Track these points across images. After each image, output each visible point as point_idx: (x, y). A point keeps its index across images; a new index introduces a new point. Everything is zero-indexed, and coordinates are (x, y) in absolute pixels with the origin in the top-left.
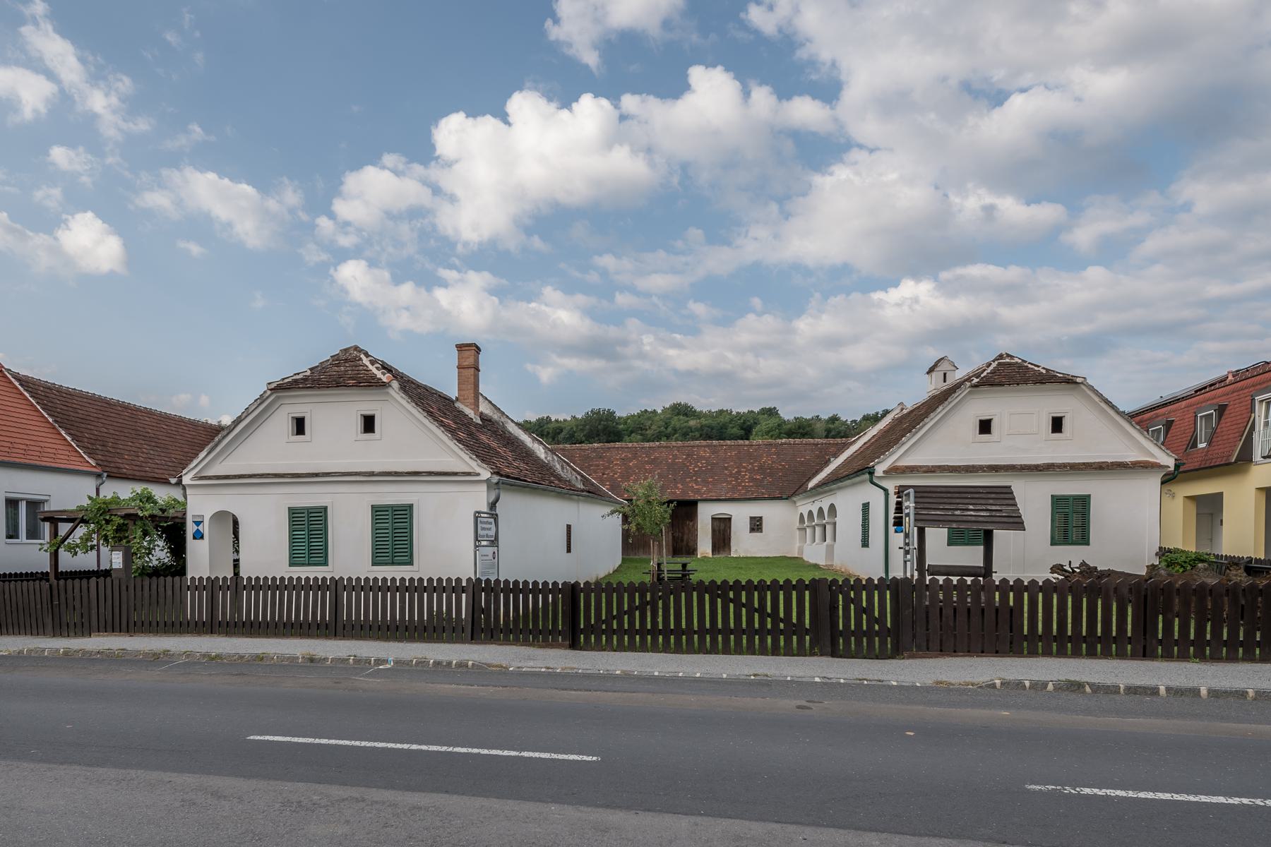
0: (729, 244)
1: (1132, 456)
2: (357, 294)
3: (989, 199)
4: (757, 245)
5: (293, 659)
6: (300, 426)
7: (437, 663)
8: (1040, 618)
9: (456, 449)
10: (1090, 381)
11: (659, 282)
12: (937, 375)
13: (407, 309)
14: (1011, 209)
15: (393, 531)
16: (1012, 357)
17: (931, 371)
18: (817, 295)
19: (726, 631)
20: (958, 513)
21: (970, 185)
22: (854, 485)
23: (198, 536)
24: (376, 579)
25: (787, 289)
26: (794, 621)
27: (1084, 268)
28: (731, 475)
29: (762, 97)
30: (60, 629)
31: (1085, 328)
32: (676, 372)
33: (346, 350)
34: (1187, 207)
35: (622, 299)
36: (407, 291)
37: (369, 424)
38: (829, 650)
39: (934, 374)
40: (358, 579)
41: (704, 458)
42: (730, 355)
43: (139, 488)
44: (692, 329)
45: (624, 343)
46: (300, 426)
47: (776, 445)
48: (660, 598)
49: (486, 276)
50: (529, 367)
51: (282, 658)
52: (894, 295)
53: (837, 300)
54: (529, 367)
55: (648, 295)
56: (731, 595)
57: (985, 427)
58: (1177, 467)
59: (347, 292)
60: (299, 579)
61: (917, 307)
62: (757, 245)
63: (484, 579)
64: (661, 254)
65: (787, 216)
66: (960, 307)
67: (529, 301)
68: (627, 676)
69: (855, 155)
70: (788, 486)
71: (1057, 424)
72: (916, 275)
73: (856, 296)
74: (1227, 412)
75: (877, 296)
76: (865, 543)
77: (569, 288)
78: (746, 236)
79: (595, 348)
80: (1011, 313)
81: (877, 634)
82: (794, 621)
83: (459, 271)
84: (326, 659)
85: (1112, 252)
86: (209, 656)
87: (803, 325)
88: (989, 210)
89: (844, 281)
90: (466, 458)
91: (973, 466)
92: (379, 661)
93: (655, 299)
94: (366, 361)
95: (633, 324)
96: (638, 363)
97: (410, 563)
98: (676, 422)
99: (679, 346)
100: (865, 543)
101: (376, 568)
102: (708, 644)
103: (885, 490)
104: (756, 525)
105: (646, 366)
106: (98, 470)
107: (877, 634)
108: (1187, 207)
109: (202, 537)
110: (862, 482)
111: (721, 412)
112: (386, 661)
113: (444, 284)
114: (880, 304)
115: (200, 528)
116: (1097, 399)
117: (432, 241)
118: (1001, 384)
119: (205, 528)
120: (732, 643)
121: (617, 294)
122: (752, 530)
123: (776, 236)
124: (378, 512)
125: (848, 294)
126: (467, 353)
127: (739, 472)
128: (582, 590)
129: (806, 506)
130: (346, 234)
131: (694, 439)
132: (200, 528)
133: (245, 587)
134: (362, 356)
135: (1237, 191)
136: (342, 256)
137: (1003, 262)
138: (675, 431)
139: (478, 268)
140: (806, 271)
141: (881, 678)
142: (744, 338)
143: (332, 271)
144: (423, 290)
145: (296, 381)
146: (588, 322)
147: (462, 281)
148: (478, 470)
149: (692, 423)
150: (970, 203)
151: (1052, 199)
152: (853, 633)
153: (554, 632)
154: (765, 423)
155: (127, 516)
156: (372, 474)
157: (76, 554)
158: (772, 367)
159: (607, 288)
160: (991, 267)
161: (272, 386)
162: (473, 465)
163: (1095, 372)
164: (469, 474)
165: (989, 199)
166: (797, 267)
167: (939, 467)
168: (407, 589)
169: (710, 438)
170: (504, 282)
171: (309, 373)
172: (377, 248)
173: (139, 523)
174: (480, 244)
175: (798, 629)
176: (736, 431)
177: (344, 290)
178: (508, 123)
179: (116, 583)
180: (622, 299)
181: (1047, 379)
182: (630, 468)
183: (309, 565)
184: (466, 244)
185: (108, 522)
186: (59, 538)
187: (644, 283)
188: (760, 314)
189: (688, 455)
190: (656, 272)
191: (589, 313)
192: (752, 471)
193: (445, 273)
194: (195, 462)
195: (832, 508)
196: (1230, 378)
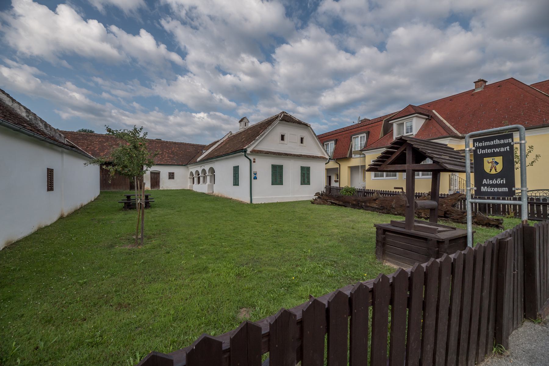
1: (319, 154)
3: (222, 97)
4: (159, 90)
10: (311, 126)
14: (226, 101)
25: (169, 107)
29: (163, 47)
35: (105, 95)
39: (242, 123)
42: (146, 123)
44: (133, 111)
45: (104, 111)
50: (56, 111)
54: (56, 111)
55: (116, 96)
57: (283, 138)
62: (159, 90)
64: (122, 84)
66: (214, 122)
69: (189, 74)
72: (205, 112)
73: (188, 113)
75: (194, 114)
76: (236, 183)
77: (79, 85)
79: (90, 110)
87: (171, 118)
95: (109, 105)
96: (109, 119)
100: (236, 183)
103: (250, 160)
104: (171, 176)
105: (113, 121)
108: (259, 111)
114: (194, 117)
122: (170, 178)
129: (193, 169)
137: (224, 114)
142: (152, 118)
150: (219, 97)
151: (235, 102)
158: (160, 129)
159: (98, 89)
163: (314, 126)
178: (56, 13)
182: (104, 146)
188: (158, 112)
195: (212, 170)
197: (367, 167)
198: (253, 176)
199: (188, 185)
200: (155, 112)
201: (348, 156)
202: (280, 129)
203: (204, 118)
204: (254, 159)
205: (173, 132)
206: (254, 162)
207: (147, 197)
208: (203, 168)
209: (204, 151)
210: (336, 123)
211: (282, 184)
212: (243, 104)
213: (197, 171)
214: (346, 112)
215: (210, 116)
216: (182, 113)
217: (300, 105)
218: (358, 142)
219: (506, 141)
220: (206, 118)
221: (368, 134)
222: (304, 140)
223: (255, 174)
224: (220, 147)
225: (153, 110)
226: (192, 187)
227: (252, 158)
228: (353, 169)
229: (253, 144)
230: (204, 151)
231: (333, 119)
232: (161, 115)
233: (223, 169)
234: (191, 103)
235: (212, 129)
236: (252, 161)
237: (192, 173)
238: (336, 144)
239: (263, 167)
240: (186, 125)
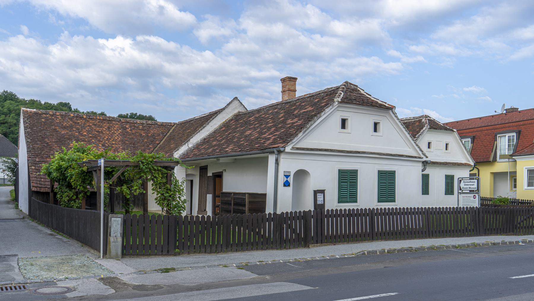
1: (464, 161)
6: (344, 123)
15: (387, 183)
24: (341, 210)
31: (203, 82)
46: (344, 123)
52: (111, 43)
61: (123, 53)
63: (465, 207)
66: (145, 58)
72: (125, 35)
73: (90, 38)
75: (102, 41)
80: (170, 67)
85: (215, 45)
87: (55, 50)
101: (380, 204)
108: (244, 31)
109: (289, 185)
114: (103, 47)
115: (288, 179)
119: (291, 180)
124: (381, 174)
125: (86, 37)
132: (288, 179)
137: (168, 40)
140: (59, 17)
142: (15, 51)
151: (191, 12)
158: (32, 73)
160: (162, 40)
168: (330, 216)
188: (27, 37)
194: (296, 139)
197: (94, 173)
200: (21, 37)
201: (491, 159)
203: (123, 50)
205: (59, 81)
210: (420, 58)
211: (428, 194)
212: (207, 16)
214: (444, 32)
215: (137, 44)
216: (76, 38)
217: (337, 16)
218: (504, 143)
220: (128, 49)
221: (519, 133)
222: (449, 147)
225: (17, 32)
228: (496, 176)
231: (413, 48)
232: (32, 43)
234: (96, 17)
235: (143, 74)
238: (473, 142)
240: (86, 66)
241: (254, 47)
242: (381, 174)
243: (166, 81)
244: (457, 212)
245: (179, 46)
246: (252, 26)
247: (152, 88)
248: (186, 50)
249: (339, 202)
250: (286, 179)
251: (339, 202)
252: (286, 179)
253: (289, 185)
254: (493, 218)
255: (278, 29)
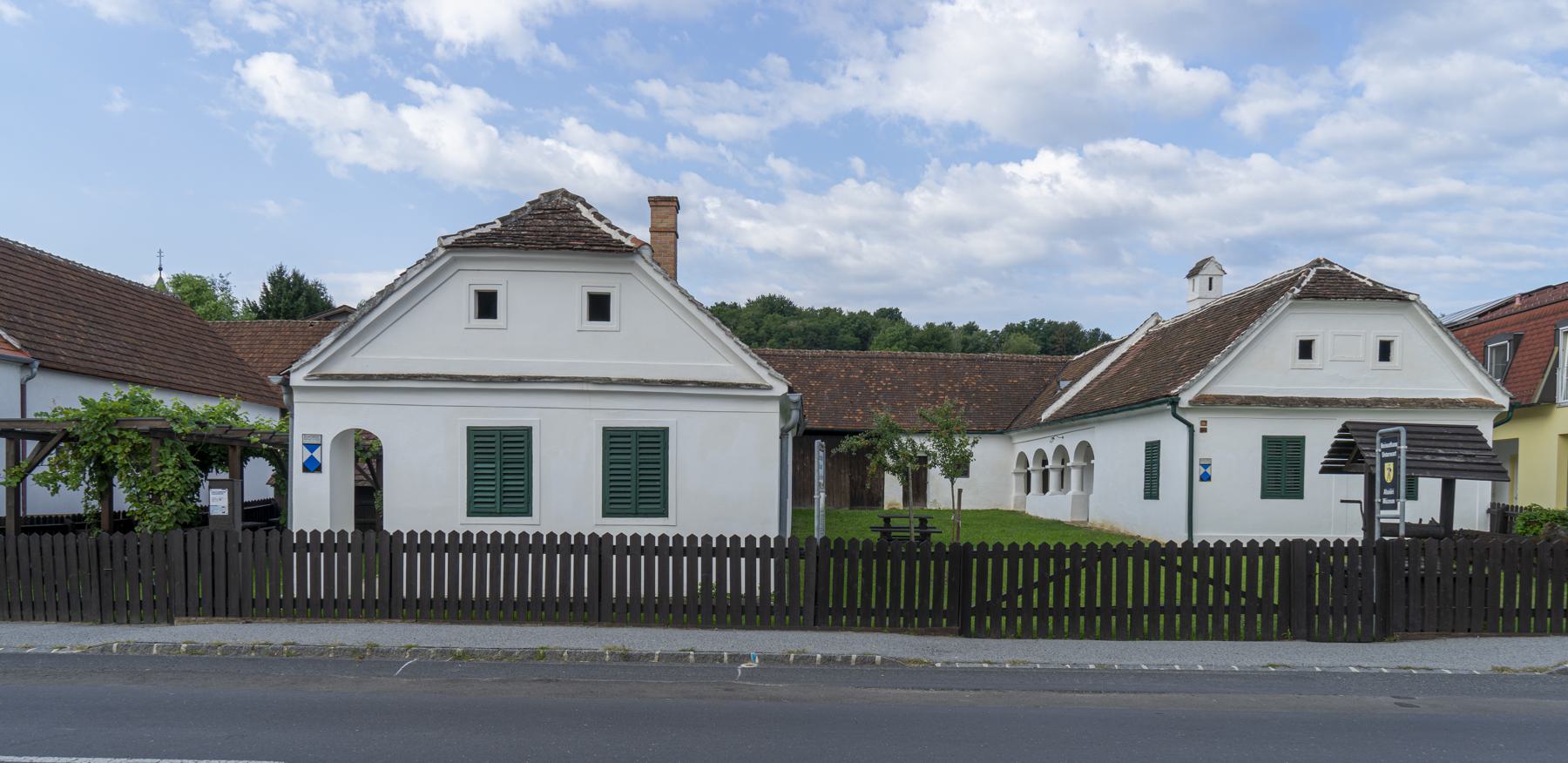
0: (822, 82)
1: (1463, 393)
2: (278, 104)
3: (1143, 58)
4: (856, 87)
5: (596, 656)
6: (487, 305)
7: (828, 660)
8: (1162, 590)
9: (737, 350)
10: (1423, 300)
11: (729, 125)
12: (1201, 280)
13: (358, 133)
14: (1168, 71)
15: (636, 466)
16: (1331, 264)
17: (1193, 274)
18: (936, 161)
19: (1170, 610)
20: (1427, 457)
21: (1120, 37)
22: (1128, 417)
23: (312, 466)
25: (898, 150)
26: (1260, 595)
27: (1248, 155)
28: (926, 399)
30: (110, 611)
31: (1249, 230)
32: (751, 252)
33: (550, 195)
34: (1359, 90)
35: (677, 146)
36: (357, 106)
37: (599, 307)
38: (1304, 631)
39: (1197, 279)
40: (735, 539)
41: (888, 374)
42: (823, 233)
43: (127, 390)
46: (487, 305)
47: (980, 361)
48: (1084, 564)
49: (480, 93)
51: (575, 655)
52: (1029, 169)
53: (961, 170)
55: (712, 142)
56: (1179, 561)
57: (1306, 350)
58: (1511, 406)
59: (263, 101)
60: (650, 538)
61: (1057, 187)
62: (856, 87)
65: (897, 51)
66: (1107, 192)
67: (543, 138)
68: (1104, 672)
70: (1009, 413)
71: (1385, 351)
72: (1057, 145)
74: (1523, 343)
75: (1010, 168)
76: (1152, 491)
77: (603, 122)
78: (844, 74)
80: (1168, 205)
81: (1243, 610)
82: (1260, 595)
83: (439, 84)
84: (650, 656)
85: (1279, 136)
86: (452, 652)
87: (918, 199)
88: (1143, 70)
89: (969, 146)
90: (752, 363)
91: (1292, 399)
92: (737, 658)
93: (722, 149)
94: (585, 213)
97: (528, 512)
98: (769, 321)
99: (755, 216)
100: (1152, 491)
102: (1082, 628)
103: (1190, 426)
105: (710, 240)
106: (25, 357)
107: (1243, 610)
108: (1359, 90)
109: (319, 469)
110: (1163, 411)
111: (827, 311)
112: (747, 658)
113: (416, 102)
114: (1013, 181)
115: (316, 454)
116: (1430, 322)
117: (398, 37)
118: (1326, 298)
119: (325, 455)
120: (1226, 625)
121: (669, 136)
123: (883, 77)
124: (615, 440)
125: (974, 164)
126: (664, 211)
127: (936, 395)
128: (614, 550)
129: (1028, 445)
130: (262, 12)
131: (796, 346)
132: (316, 454)
133: (294, 547)
134: (579, 205)
135: (1412, 76)
136: (256, 44)
137: (1158, 141)
138: (770, 334)
139: (467, 82)
140: (924, 130)
141: (1430, 665)
142: (843, 212)
143: (238, 66)
144: (383, 107)
145: (483, 236)
146: (628, 173)
147: (443, 98)
148: (769, 381)
149: (792, 324)
151: (1213, 65)
152: (1211, 610)
153: (937, 612)
154: (888, 331)
155: (152, 433)
156: (608, 381)
157: (56, 490)
158: (877, 253)
159: (655, 128)
160: (1145, 144)
161: (449, 241)
162: (764, 375)
164: (756, 387)
165: (1143, 58)
166: (911, 122)
167: (1254, 398)
169: (817, 346)
170: (506, 106)
171: (498, 225)
172: (312, 38)
173: (169, 442)
174: (471, 47)
175: (1263, 606)
176: (849, 338)
177: (258, 96)
179: (220, 539)
180: (677, 146)
181: (1377, 294)
183: (501, 514)
184: (449, 45)
185: (115, 440)
186: (24, 464)
187: (706, 126)
188: (862, 181)
189: (866, 370)
190: (723, 111)
191: (630, 160)
192: (952, 395)
193: (425, 89)
194: (314, 352)
195: (1086, 451)
196: (1518, 303)
198: (1199, 472)
199: (1010, 497)
200: (851, 183)
202: (1292, 324)
203: (1056, 178)
204: (1204, 423)
206: (1203, 430)
207: (923, 521)
208: (1058, 442)
209: (1063, 384)
211: (1301, 497)
213: (1040, 454)
219: (1391, 445)
223: (1205, 466)
224: (1113, 371)
226: (1024, 503)
227: (1195, 420)
229: (1199, 379)
230: (1063, 384)
232: (875, 192)
233: (1117, 446)
235: (1102, 232)
236: (1197, 427)
237: (1022, 459)
239: (1236, 447)
240: (984, 224)
241: (1388, 126)
242: (615, 440)
243: (1158, 239)
244: (1297, 557)
245: (1187, 153)
246: (1378, 75)
247: (1127, 258)
248: (1206, 160)
249: (471, 513)
250: (308, 454)
251: (471, 513)
252: (308, 454)
253: (319, 469)
254: (867, 575)
255: (1459, 67)
